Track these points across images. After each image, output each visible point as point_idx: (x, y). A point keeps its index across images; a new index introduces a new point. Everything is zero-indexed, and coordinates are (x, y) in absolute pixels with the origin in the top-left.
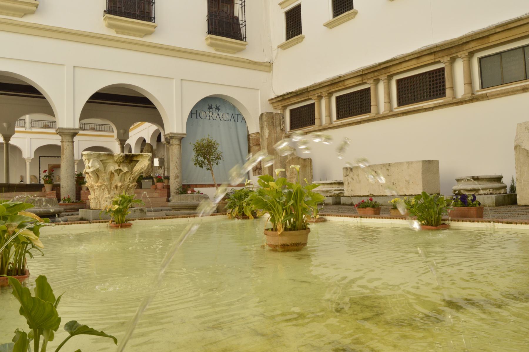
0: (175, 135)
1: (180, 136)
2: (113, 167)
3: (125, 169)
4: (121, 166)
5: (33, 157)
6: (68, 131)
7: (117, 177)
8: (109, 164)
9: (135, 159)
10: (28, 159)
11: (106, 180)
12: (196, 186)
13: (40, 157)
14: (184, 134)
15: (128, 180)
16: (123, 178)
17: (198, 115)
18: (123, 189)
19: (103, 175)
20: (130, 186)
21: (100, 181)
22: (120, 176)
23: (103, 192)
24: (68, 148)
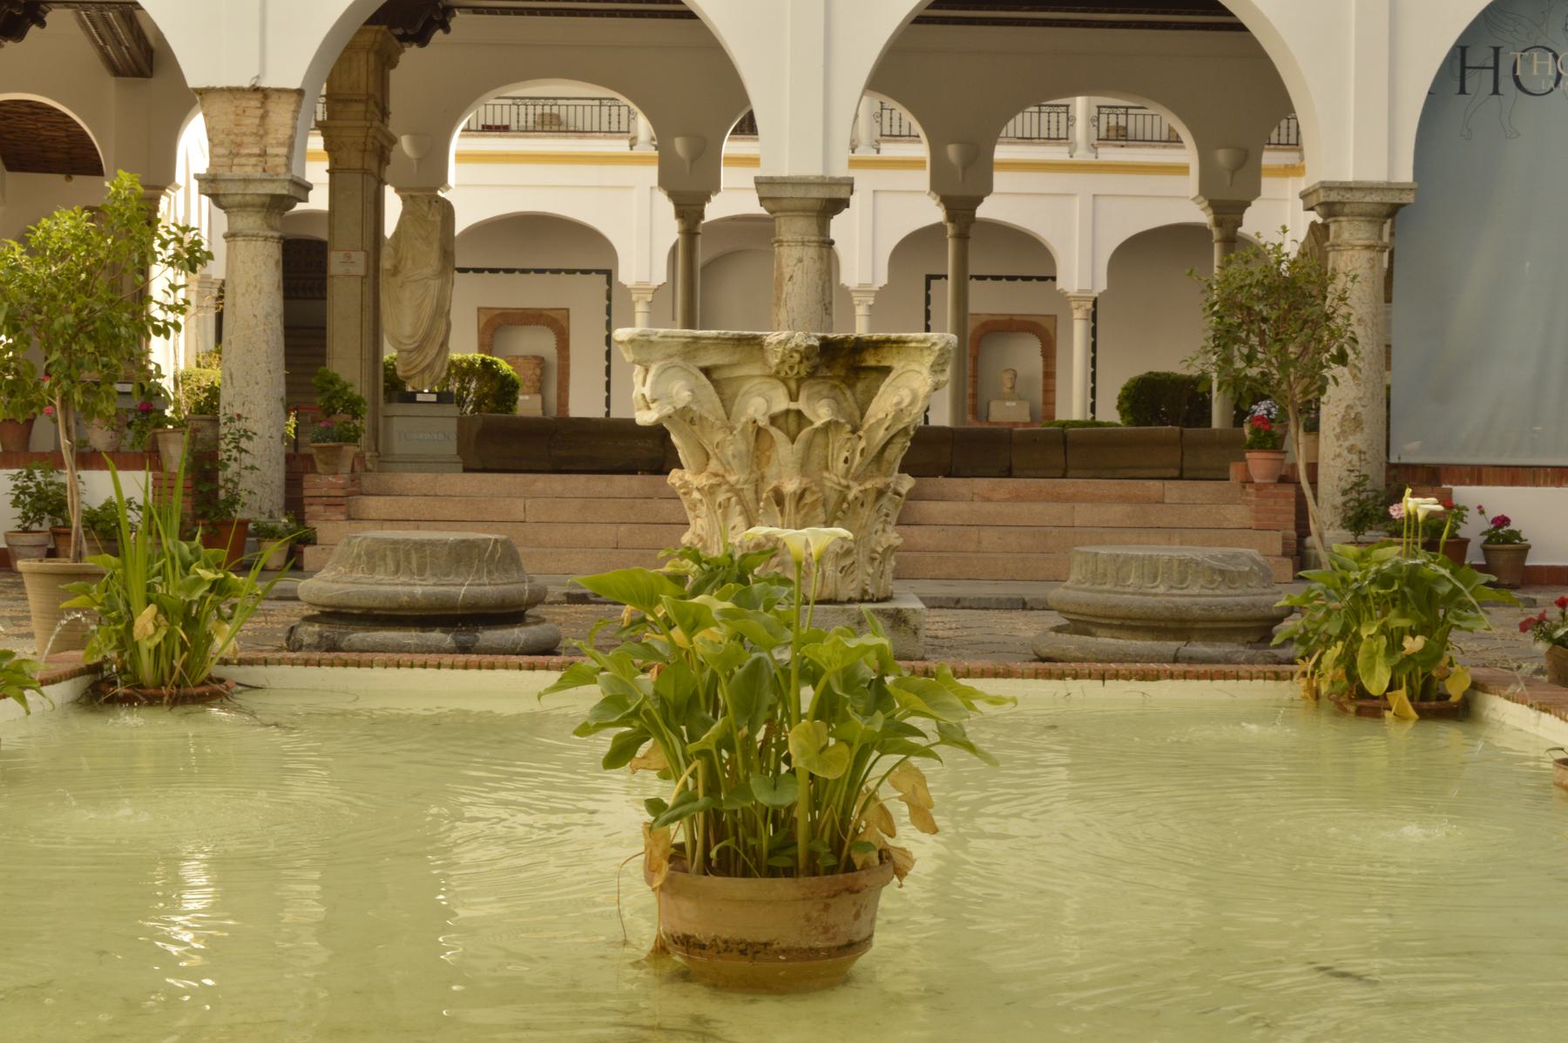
0: (1348, 196)
1: (1375, 198)
2: (762, 401)
3: (821, 413)
4: (803, 395)
5: (882, 279)
6: (800, 193)
7: (785, 451)
8: (747, 386)
9: (871, 361)
10: (863, 289)
11: (735, 463)
12: (1477, 475)
13: (929, 278)
14: (1402, 189)
15: (841, 466)
16: (817, 453)
17: (1506, 70)
18: (813, 505)
19: (719, 437)
20: (851, 496)
21: (714, 465)
22: (798, 445)
23: (725, 517)
24: (798, 276)
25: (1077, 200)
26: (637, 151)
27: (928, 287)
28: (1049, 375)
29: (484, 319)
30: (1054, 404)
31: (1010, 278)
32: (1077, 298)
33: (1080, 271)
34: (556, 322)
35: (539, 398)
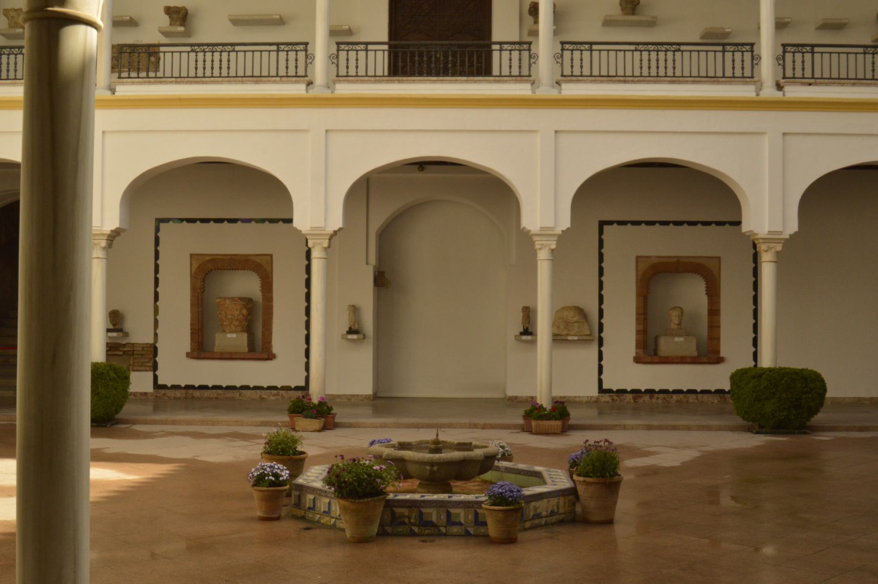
10: (545, 233)
13: (602, 224)
25: (766, 140)
26: (314, 92)
27: (601, 232)
28: (714, 312)
29: (195, 265)
30: (719, 339)
31: (677, 223)
32: (766, 240)
33: (769, 211)
34: (261, 267)
35: (245, 336)
